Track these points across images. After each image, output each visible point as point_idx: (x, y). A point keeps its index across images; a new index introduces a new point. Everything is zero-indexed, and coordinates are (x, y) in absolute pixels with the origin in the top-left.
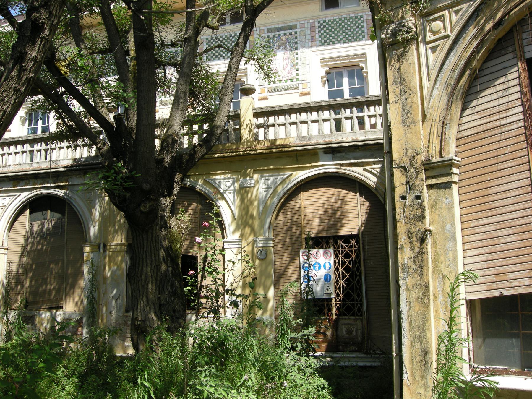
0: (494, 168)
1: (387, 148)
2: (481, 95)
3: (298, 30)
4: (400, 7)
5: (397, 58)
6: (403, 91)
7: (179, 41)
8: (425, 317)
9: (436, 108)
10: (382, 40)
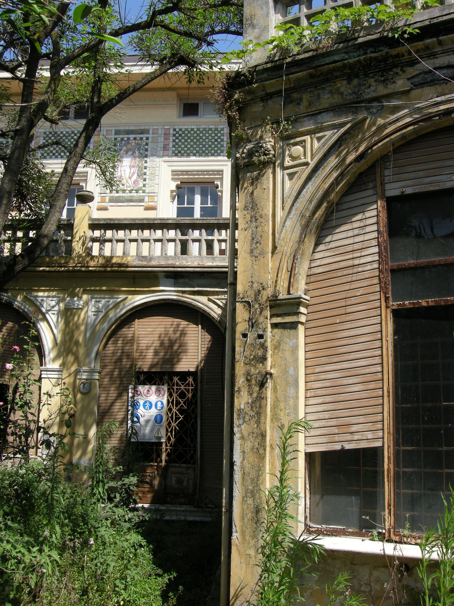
0: (342, 311)
1: (232, 279)
2: (337, 231)
3: (150, 136)
4: (260, 126)
5: (251, 181)
6: (254, 218)
7: (11, 131)
8: (259, 470)
9: (288, 240)
10: (237, 159)
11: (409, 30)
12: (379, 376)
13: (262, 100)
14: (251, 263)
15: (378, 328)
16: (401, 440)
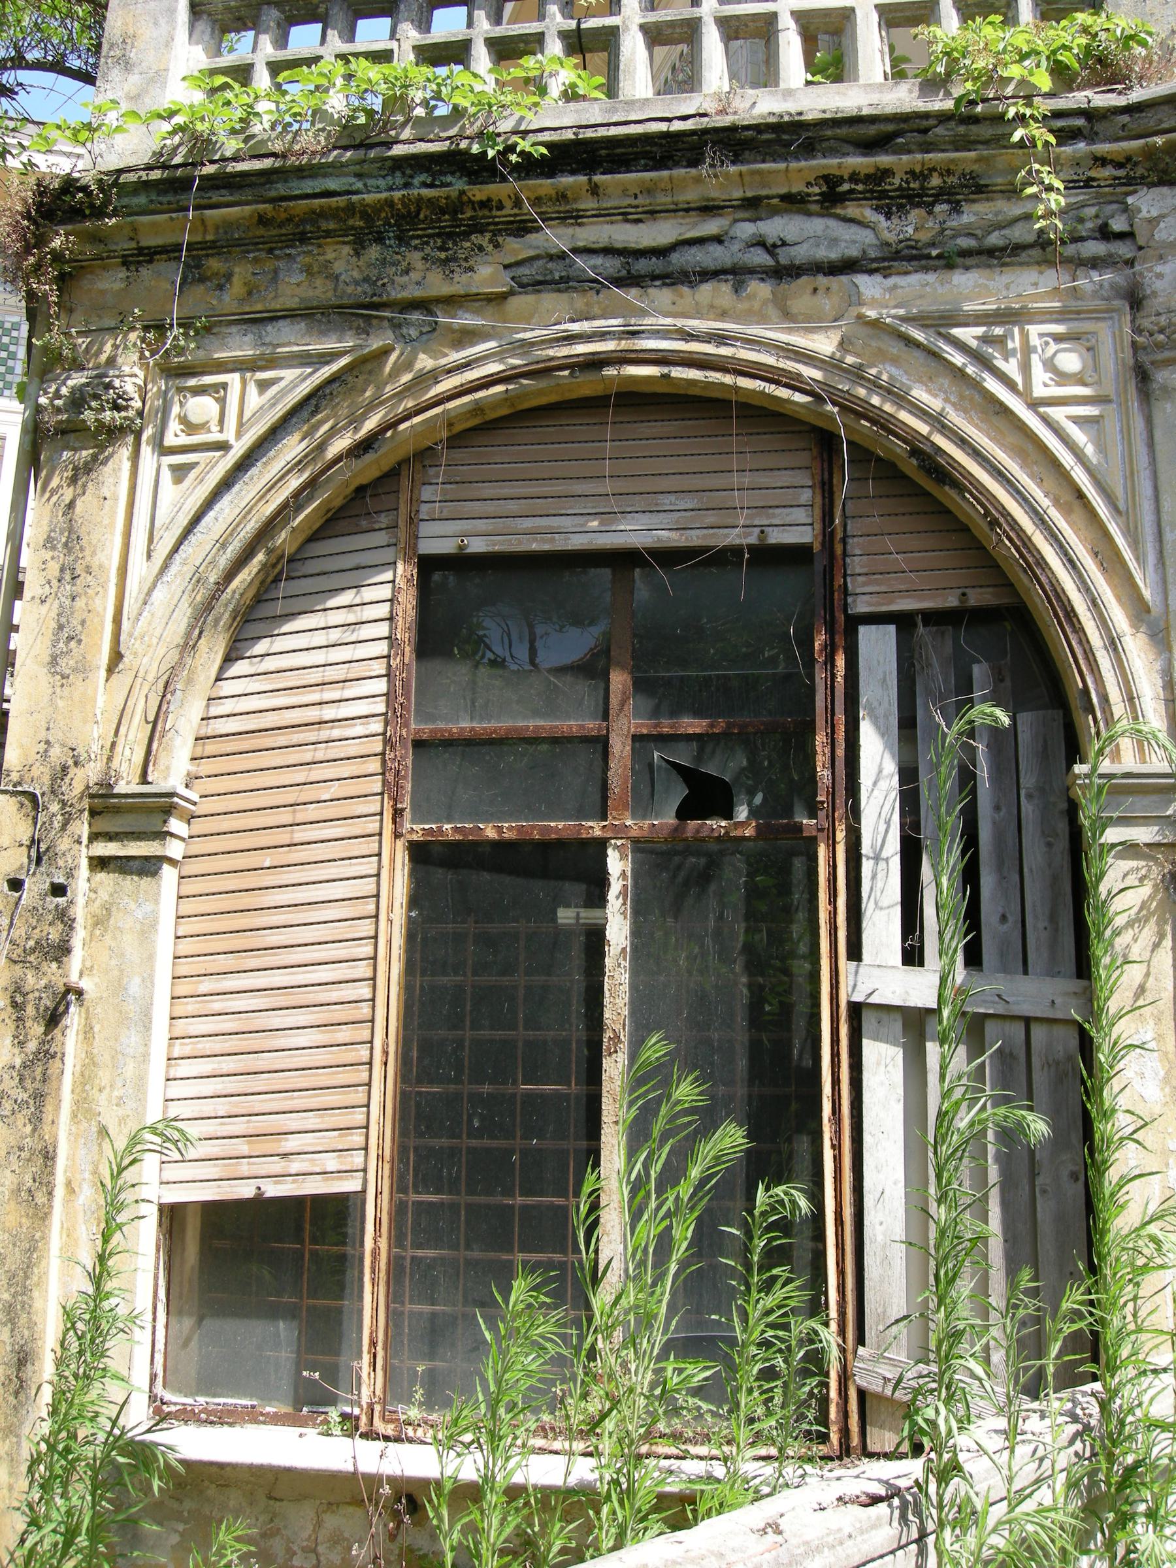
0: (283, 836)
2: (285, 629)
5: (70, 473)
6: (69, 574)
8: (32, 1249)
9: (155, 641)
10: (39, 409)
11: (524, 145)
12: (365, 1010)
13: (125, 264)
14: (50, 691)
15: (369, 886)
16: (411, 1177)
